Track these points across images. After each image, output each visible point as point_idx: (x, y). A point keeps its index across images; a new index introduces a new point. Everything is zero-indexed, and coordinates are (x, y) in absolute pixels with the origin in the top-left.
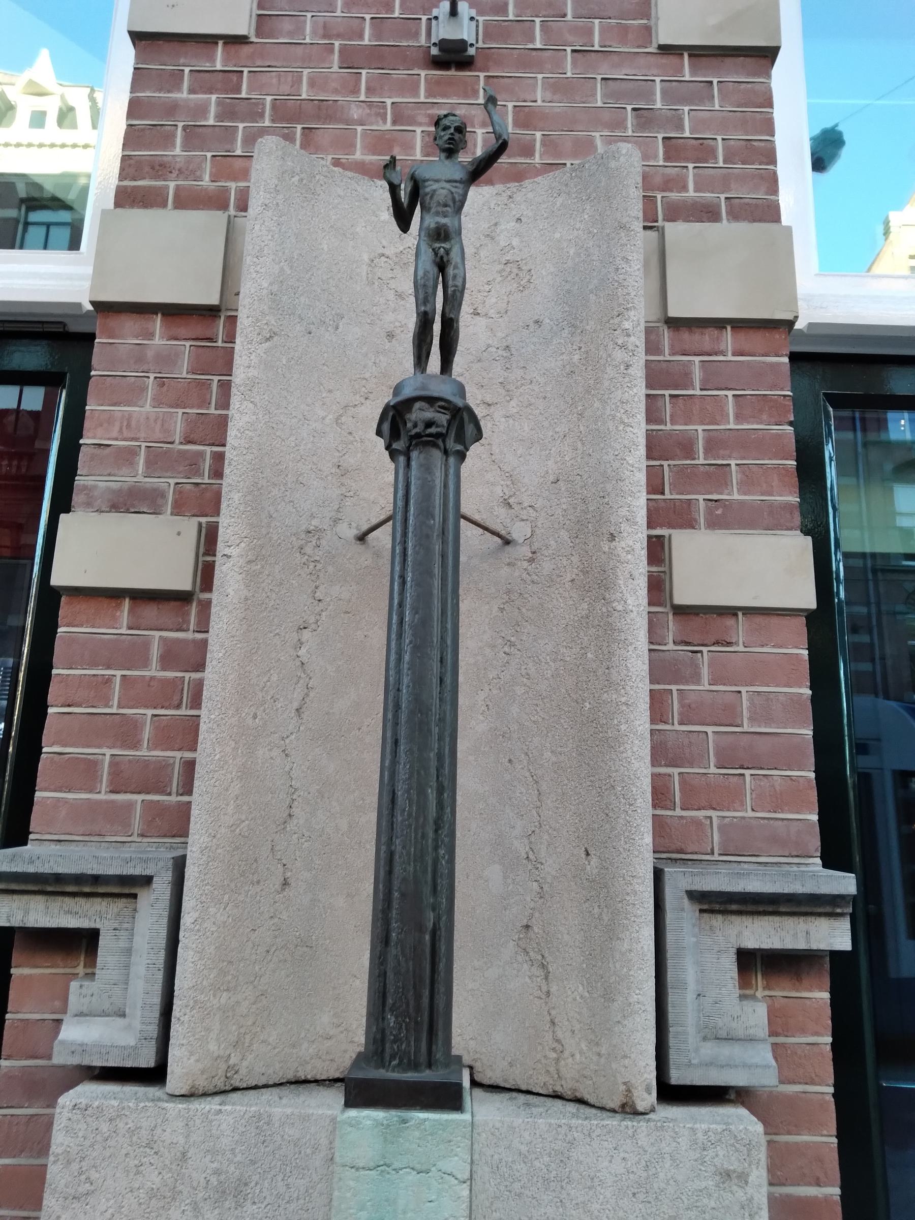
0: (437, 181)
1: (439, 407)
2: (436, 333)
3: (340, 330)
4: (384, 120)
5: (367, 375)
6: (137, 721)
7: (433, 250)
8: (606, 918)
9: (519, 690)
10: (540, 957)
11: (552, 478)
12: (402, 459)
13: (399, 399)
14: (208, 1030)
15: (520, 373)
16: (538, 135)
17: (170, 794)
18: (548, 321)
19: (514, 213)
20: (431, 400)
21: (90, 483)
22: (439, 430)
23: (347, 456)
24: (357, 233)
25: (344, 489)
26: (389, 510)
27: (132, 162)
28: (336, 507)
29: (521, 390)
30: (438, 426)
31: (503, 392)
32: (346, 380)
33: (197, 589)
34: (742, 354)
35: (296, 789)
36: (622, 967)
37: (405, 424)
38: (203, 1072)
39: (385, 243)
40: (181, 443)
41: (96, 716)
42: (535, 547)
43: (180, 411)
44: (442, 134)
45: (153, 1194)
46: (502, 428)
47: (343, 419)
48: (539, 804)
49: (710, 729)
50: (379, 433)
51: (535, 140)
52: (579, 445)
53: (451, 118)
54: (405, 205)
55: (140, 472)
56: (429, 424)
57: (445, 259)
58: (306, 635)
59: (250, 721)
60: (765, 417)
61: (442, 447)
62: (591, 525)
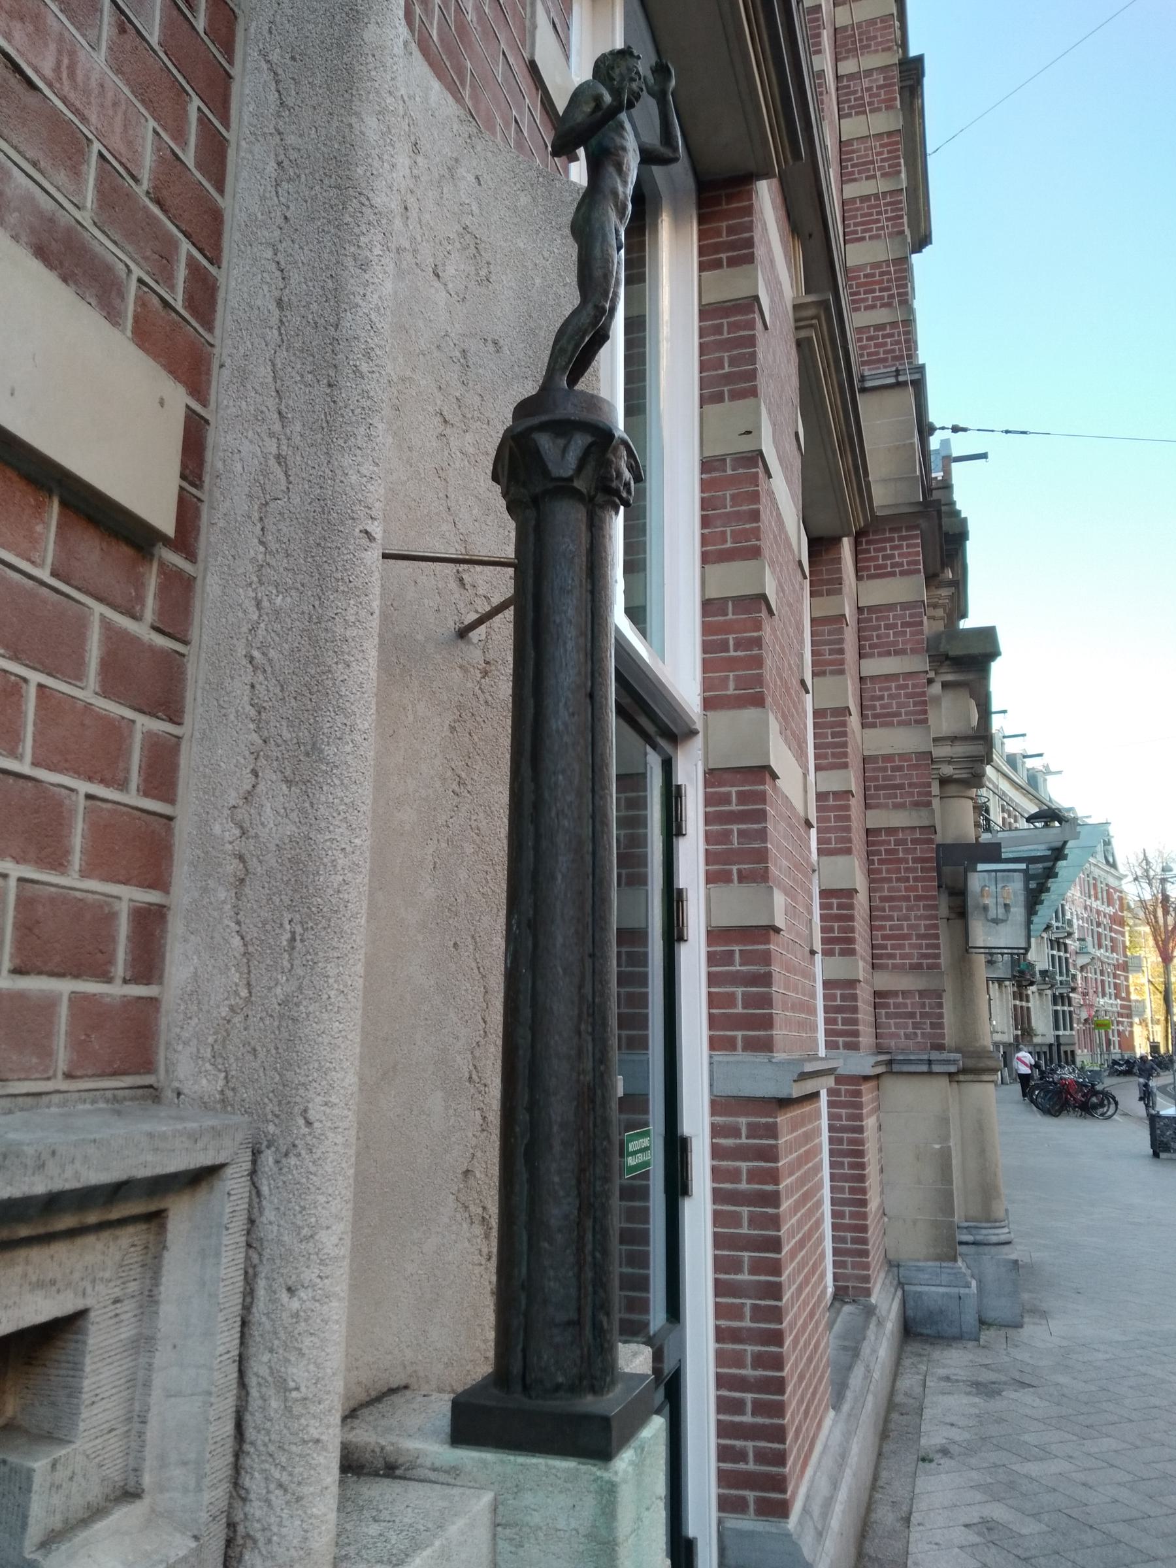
9: (469, 849)
10: (480, 1211)
17: (109, 980)
34: (159, 203)
41: (21, 782)
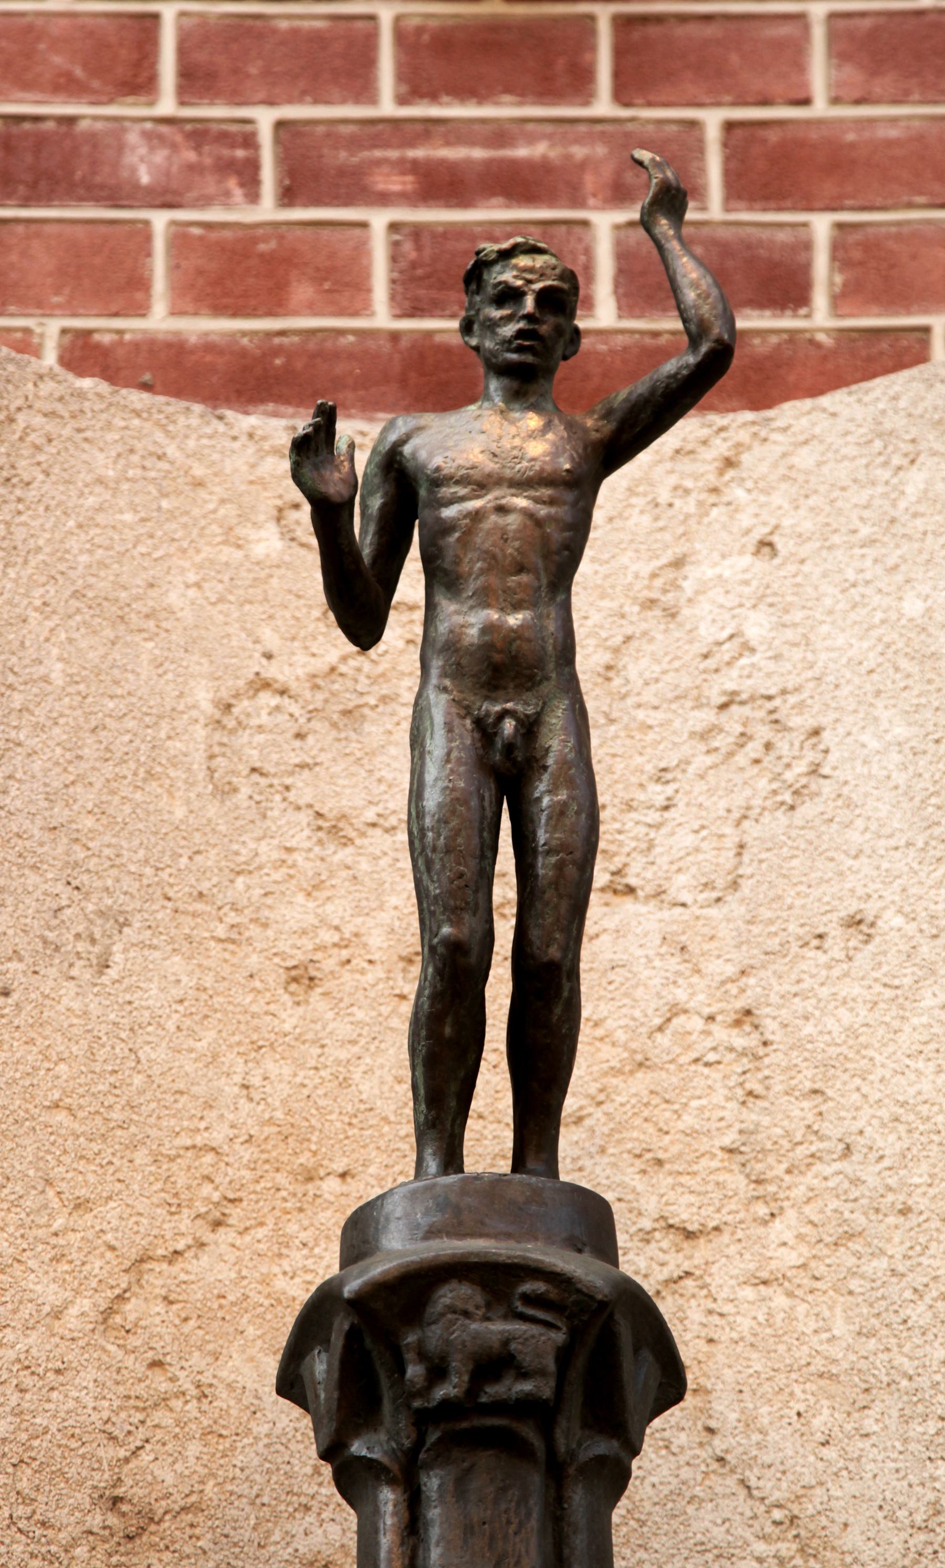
0: (481, 485)
1: (528, 1299)
2: (500, 997)
3: (113, 973)
5: (218, 1136)
7: (479, 723)
13: (377, 1269)
16: (821, 225)
18: (898, 921)
19: (745, 520)
20: (496, 1280)
22: (527, 1387)
23: (146, 1457)
29: (809, 1179)
30: (523, 1375)
31: (737, 1182)
32: (141, 1157)
39: (270, 638)
44: (496, 313)
46: (745, 1324)
47: (132, 1309)
50: (290, 1385)
51: (807, 246)
53: (523, 261)
54: (366, 552)
56: (494, 1363)
57: (519, 756)
61: (541, 1453)
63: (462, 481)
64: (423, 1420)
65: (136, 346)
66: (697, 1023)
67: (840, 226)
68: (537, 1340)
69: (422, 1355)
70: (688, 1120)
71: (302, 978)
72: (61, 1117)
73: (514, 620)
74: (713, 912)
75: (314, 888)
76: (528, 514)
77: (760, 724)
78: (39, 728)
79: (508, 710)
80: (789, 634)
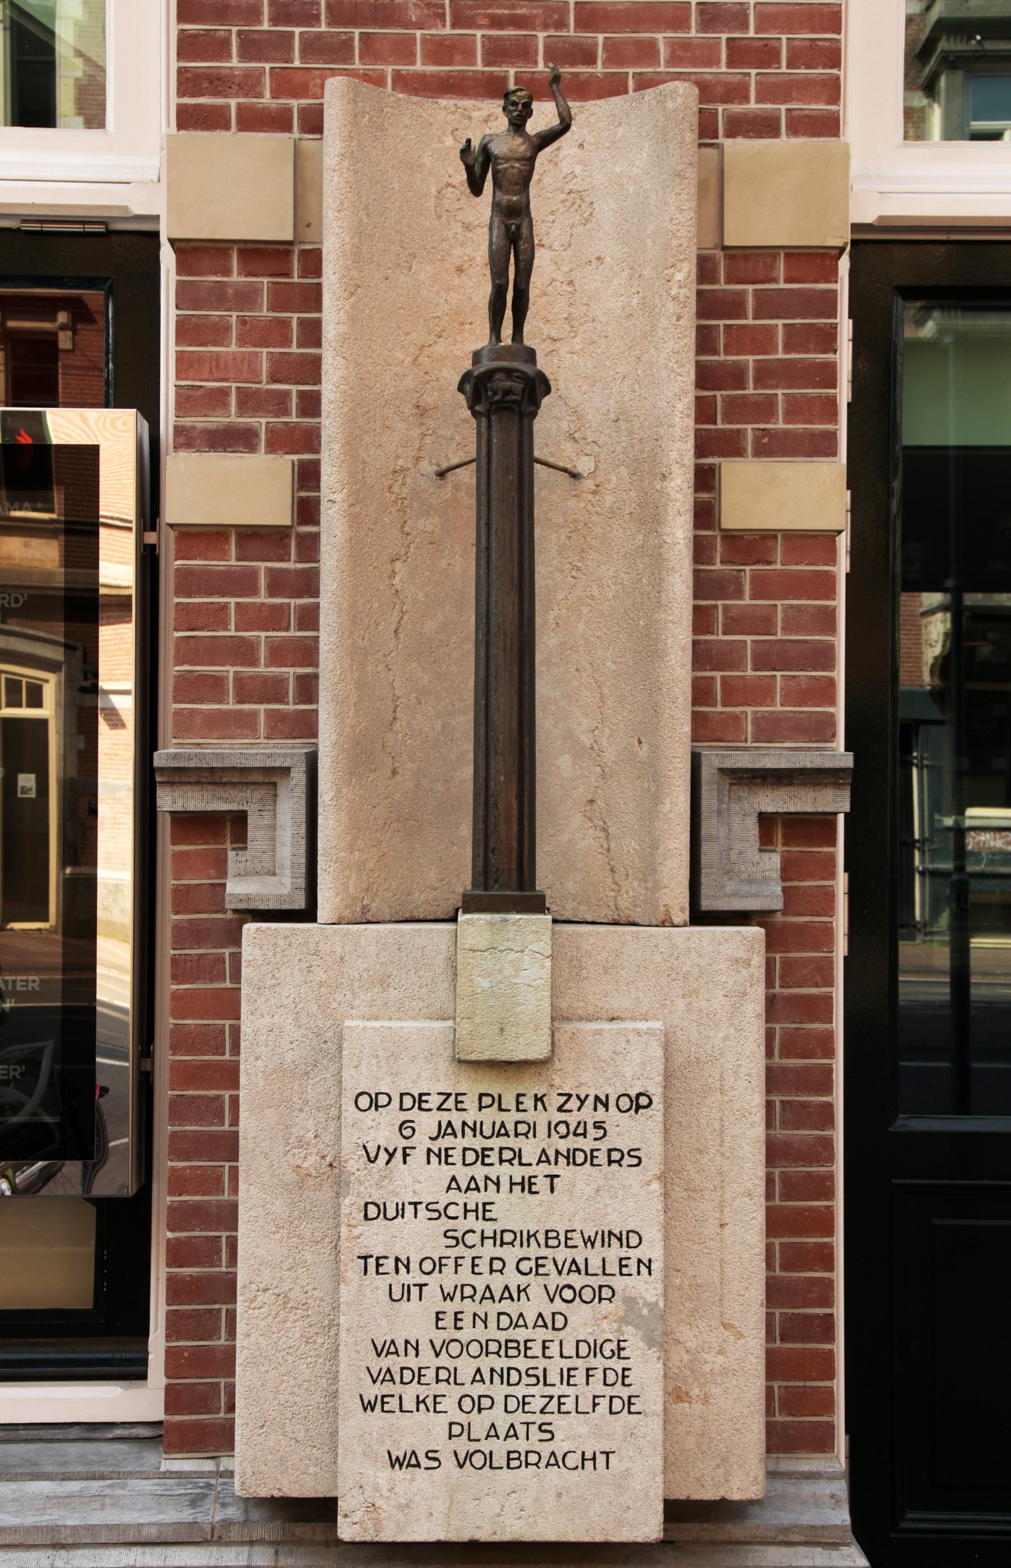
1: (516, 377)
2: (510, 295)
4: (444, 26)
5: (439, 314)
6: (253, 642)
8: (653, 789)
9: (585, 610)
10: (602, 823)
11: (613, 417)
12: (484, 420)
13: (482, 369)
14: (348, 877)
15: (584, 309)
16: (601, 37)
19: (576, 137)
20: (508, 372)
21: (188, 424)
22: (515, 397)
24: (424, 164)
25: (423, 427)
26: (474, 456)
27: (189, 75)
28: (418, 446)
29: (584, 327)
30: (514, 394)
31: (567, 327)
32: (421, 320)
33: (295, 523)
35: (398, 698)
36: (664, 824)
37: (487, 391)
38: (346, 908)
39: (451, 171)
40: (268, 383)
42: (599, 480)
43: (265, 350)
45: (321, 984)
46: (567, 363)
47: (420, 359)
48: (601, 704)
49: (749, 638)
50: (461, 389)
51: (597, 45)
52: (637, 386)
55: (233, 412)
56: (508, 392)
58: (398, 565)
59: (360, 641)
60: (811, 346)
62: (647, 468)
63: (503, 159)
64: (491, 404)
65: (412, 75)
66: (559, 284)
67: (605, 38)
68: (517, 386)
69: (492, 389)
70: (556, 310)
71: (460, 270)
72: (402, 311)
73: (515, 199)
74: (564, 253)
75: (462, 244)
76: (519, 169)
77: (577, 199)
78: (393, 203)
79: (513, 222)
80: (586, 173)
